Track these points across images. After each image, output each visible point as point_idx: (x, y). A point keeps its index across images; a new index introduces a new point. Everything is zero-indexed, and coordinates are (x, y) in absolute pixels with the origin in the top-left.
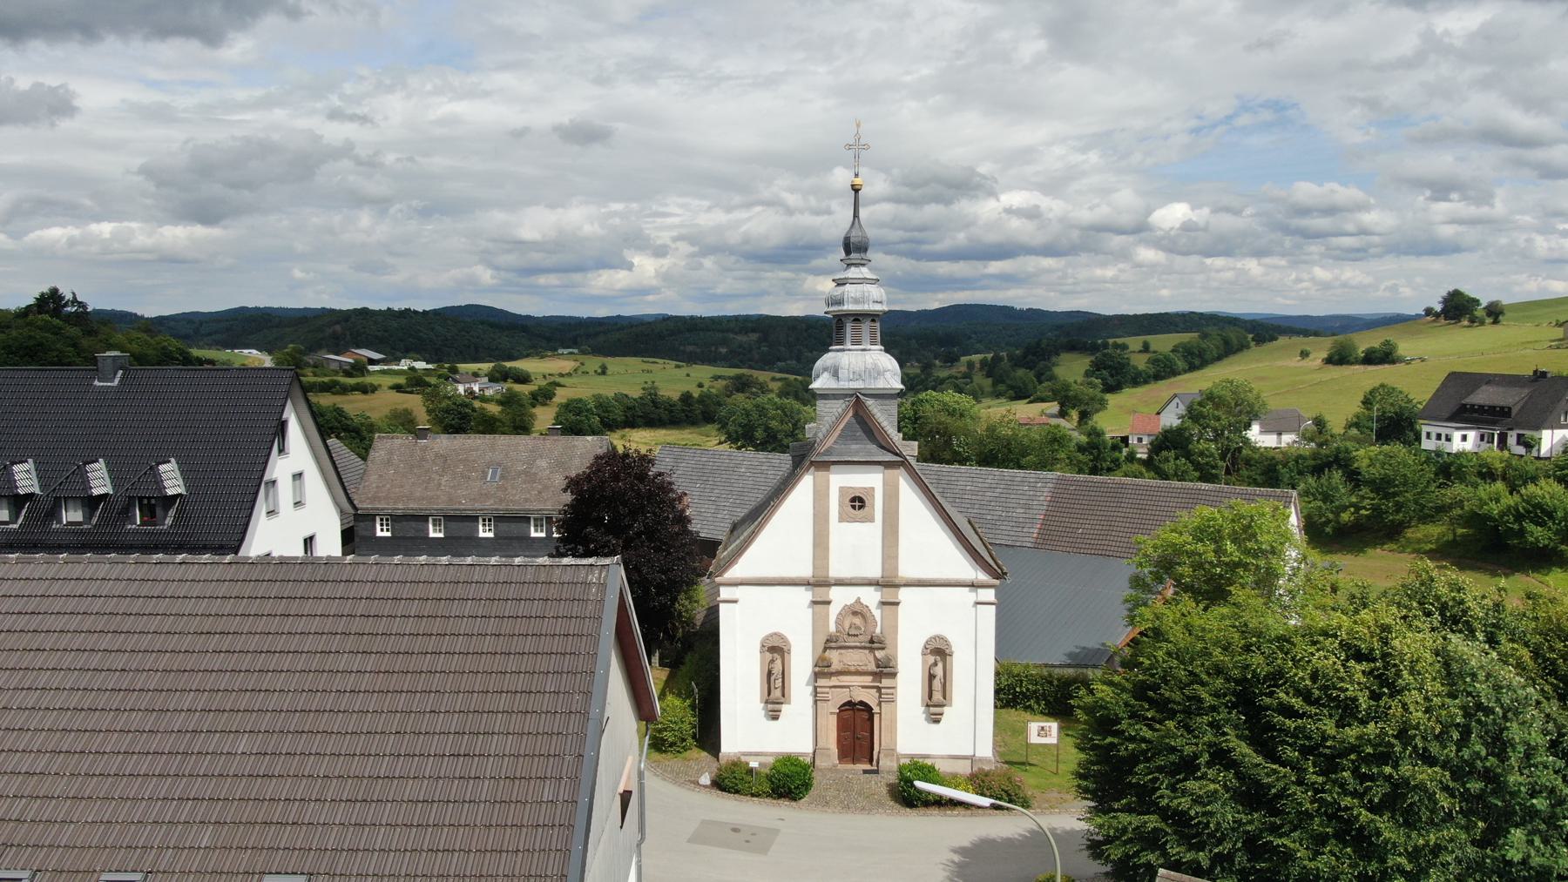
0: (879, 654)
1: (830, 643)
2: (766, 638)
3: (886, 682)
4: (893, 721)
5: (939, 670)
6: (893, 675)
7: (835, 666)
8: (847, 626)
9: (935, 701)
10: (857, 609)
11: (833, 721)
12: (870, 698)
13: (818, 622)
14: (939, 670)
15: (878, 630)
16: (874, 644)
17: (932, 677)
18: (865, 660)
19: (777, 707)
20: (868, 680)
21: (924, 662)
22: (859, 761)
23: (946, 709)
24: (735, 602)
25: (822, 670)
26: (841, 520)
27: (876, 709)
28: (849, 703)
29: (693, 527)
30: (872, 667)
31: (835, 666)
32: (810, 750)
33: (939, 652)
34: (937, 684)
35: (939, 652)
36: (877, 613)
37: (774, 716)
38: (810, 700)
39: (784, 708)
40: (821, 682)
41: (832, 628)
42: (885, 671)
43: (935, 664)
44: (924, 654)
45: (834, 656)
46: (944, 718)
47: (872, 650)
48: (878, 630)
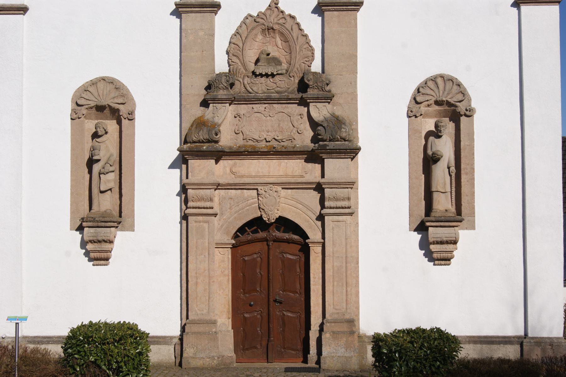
0: (319, 112)
1: (216, 91)
2: (85, 89)
3: (335, 167)
4: (351, 261)
5: (445, 147)
6: (352, 152)
7: (226, 139)
8: (251, 55)
9: (438, 221)
10: (273, 19)
11: (223, 260)
12: (299, 208)
13: (192, 50)
14: (445, 147)
15: (316, 67)
16: (307, 90)
17: (430, 161)
18: (292, 124)
19: (103, 233)
20: (295, 168)
21: (412, 132)
22: (281, 357)
23: (463, 235)
24: (23, 10)
25: (198, 145)
26: (307, 363)
27: (314, 235)
28: (257, 224)
29: (149, 354)
30: (305, 138)
31: (226, 139)
32: (176, 332)
33: (444, 109)
34: (441, 173)
35: (444, 109)
36: (312, 26)
37: (98, 253)
38: (174, 205)
39: (121, 238)
40: (203, 169)
41: (221, 65)
42: (332, 142)
43: (436, 134)
44: (411, 115)
45: (229, 124)
46: (459, 253)
47: (304, 103)
48: (316, 67)
